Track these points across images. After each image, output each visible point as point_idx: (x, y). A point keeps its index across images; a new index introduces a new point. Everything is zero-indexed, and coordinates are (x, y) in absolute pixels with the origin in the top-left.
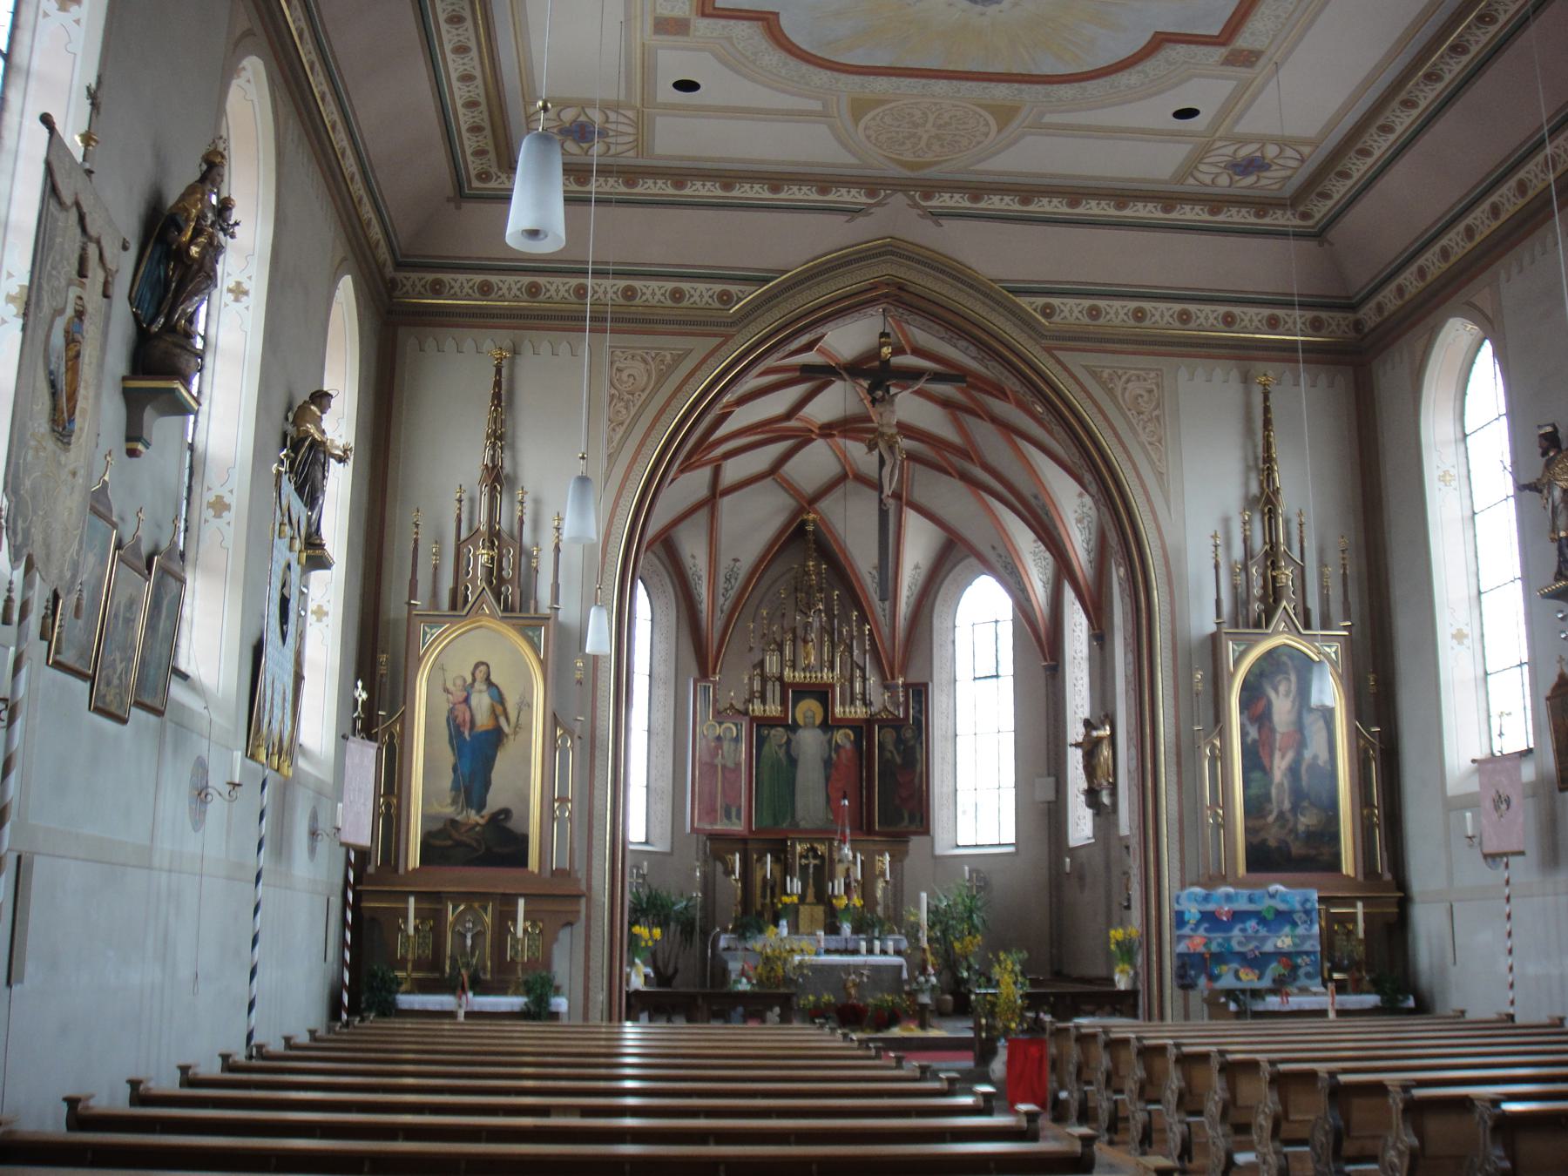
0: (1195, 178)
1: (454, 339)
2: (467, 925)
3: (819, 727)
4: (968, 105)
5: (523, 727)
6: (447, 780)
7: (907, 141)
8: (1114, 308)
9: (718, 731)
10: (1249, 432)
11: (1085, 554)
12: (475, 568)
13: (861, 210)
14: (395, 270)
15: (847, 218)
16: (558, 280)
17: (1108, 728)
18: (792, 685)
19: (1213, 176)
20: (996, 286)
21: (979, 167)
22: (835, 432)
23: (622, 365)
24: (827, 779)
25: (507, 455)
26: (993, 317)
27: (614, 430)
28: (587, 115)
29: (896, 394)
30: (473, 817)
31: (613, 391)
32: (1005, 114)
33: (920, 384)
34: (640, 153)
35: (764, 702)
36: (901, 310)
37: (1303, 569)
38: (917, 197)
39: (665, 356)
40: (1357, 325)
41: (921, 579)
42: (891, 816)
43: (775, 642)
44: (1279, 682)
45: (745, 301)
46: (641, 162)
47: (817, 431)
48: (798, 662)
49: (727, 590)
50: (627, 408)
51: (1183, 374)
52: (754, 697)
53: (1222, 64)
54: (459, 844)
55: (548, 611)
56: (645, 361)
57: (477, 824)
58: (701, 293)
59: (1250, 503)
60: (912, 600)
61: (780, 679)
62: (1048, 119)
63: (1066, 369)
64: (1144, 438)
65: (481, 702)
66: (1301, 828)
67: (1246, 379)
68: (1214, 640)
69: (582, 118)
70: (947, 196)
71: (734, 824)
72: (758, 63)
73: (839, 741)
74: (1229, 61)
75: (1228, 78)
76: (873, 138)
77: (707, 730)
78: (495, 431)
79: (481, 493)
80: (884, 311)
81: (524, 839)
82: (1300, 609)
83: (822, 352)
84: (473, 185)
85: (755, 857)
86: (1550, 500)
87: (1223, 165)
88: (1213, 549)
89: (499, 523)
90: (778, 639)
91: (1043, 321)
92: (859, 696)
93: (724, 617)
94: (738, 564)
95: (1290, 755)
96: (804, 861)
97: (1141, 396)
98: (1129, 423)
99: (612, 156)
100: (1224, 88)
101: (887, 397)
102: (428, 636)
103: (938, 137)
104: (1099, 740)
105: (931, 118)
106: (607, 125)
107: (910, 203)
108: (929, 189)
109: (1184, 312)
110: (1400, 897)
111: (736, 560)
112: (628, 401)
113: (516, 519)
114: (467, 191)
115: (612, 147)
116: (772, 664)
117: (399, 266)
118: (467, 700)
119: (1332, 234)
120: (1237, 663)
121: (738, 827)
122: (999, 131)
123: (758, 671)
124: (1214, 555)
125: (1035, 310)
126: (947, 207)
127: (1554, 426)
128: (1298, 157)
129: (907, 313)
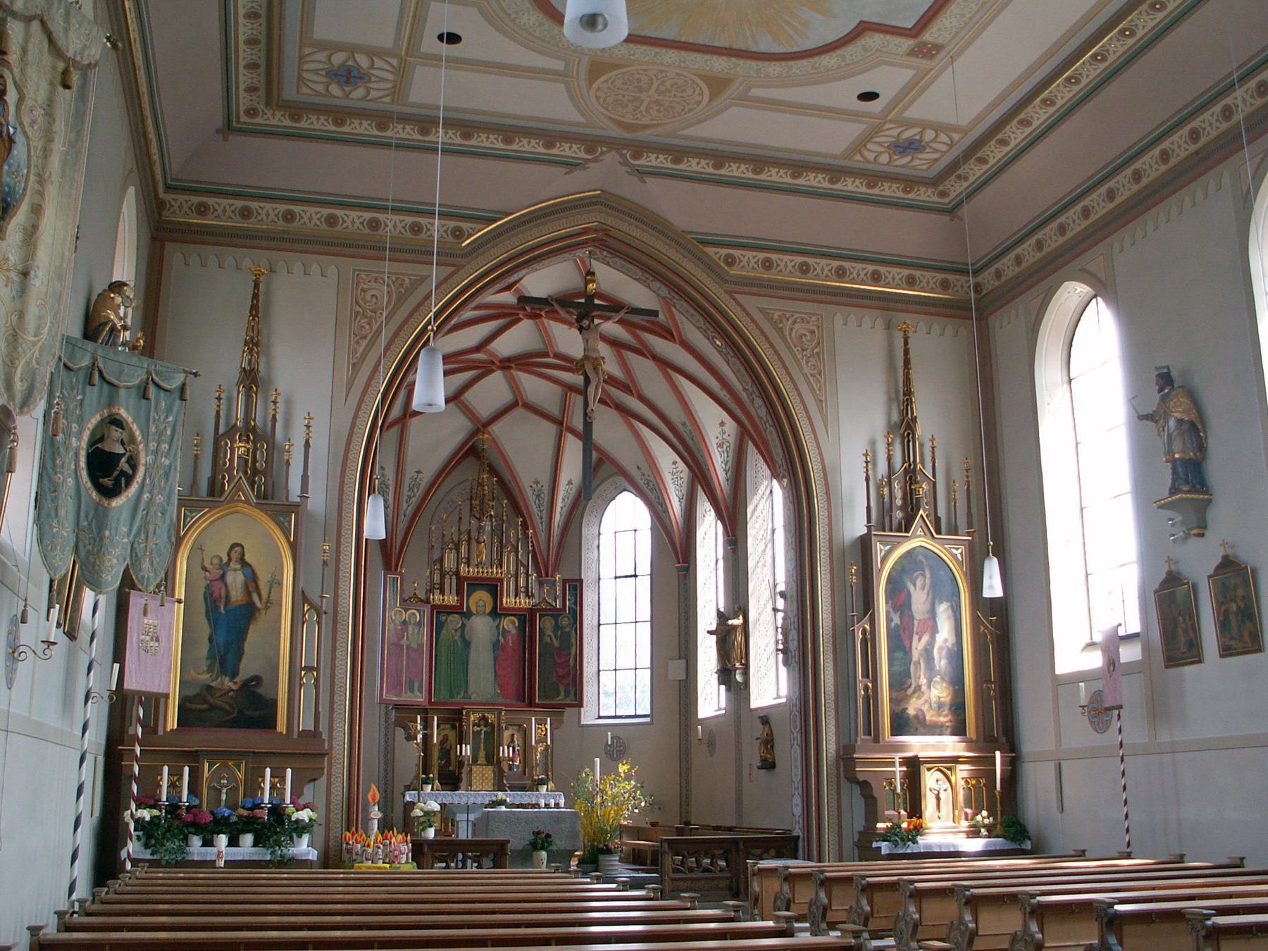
0: (862, 155)
2: (222, 781)
3: (488, 614)
4: (690, 75)
5: (273, 603)
6: (203, 649)
7: (630, 105)
9: (405, 616)
11: (724, 473)
12: (231, 460)
14: (165, 193)
17: (741, 617)
18: (466, 578)
19: (876, 154)
21: (686, 132)
22: (513, 365)
24: (495, 659)
25: (262, 360)
26: (685, 263)
27: (358, 343)
30: (227, 683)
31: (358, 309)
32: (718, 85)
33: (621, 314)
34: (396, 100)
35: (442, 592)
36: (605, 253)
37: (934, 484)
38: (628, 155)
39: (404, 280)
42: (548, 692)
43: (453, 542)
44: (917, 577)
45: (475, 237)
46: (396, 108)
47: (498, 363)
48: (472, 561)
52: (434, 588)
53: (909, 54)
54: (213, 708)
55: (298, 500)
59: (891, 429)
61: (457, 573)
62: (755, 92)
63: (744, 309)
64: (807, 371)
65: (236, 579)
66: (934, 700)
67: (888, 327)
68: (865, 544)
69: (350, 63)
70: (653, 156)
71: (418, 697)
72: (517, 21)
73: (505, 627)
74: (912, 53)
75: (910, 67)
77: (395, 615)
78: (252, 338)
79: (239, 392)
80: (590, 253)
81: (274, 704)
82: (932, 518)
84: (241, 120)
86: (1166, 429)
87: (886, 145)
88: (865, 465)
89: (254, 420)
90: (456, 539)
93: (407, 520)
94: (420, 476)
95: (925, 638)
96: (476, 729)
97: (805, 335)
98: (795, 356)
99: (371, 100)
100: (907, 75)
102: (189, 519)
103: (657, 102)
104: (734, 627)
105: (656, 84)
106: (372, 72)
107: (622, 161)
108: (640, 149)
109: (840, 268)
110: (1012, 757)
111: (418, 472)
112: (371, 317)
113: (270, 417)
114: (234, 124)
115: (372, 92)
116: (450, 561)
117: (168, 188)
119: (965, 210)
120: (884, 560)
121: (420, 698)
122: (710, 100)
123: (438, 566)
126: (652, 167)
127: (1168, 367)
129: (609, 255)
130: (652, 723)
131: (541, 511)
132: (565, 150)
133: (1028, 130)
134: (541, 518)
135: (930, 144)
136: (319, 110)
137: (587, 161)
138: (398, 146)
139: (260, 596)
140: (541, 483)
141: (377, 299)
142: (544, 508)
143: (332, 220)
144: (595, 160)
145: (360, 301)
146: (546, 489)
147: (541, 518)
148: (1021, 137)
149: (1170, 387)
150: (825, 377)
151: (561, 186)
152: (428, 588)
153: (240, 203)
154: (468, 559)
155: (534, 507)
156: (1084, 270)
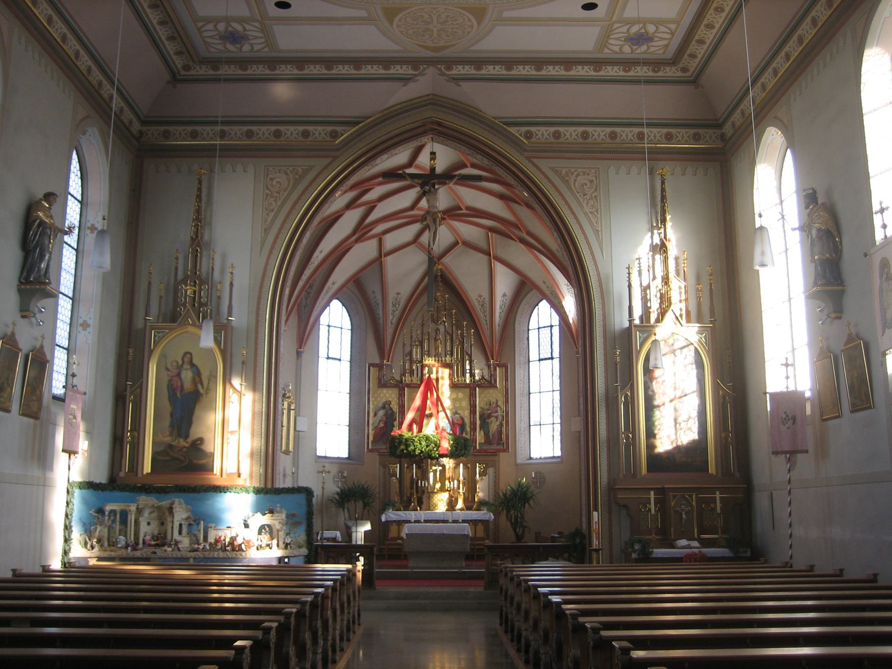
0: (609, 49)
1: (232, 165)
6: (167, 422)
8: (653, 133)
10: (653, 204)
13: (411, 78)
15: (403, 84)
16: (543, 129)
19: (619, 47)
20: (496, 121)
23: (273, 176)
27: (268, 214)
28: (232, 27)
29: (439, 188)
30: (182, 443)
31: (268, 192)
39: (298, 170)
40: (722, 137)
41: (507, 303)
46: (273, 54)
49: (394, 311)
50: (276, 201)
51: (612, 170)
56: (286, 173)
57: (185, 447)
58: (320, 132)
60: (503, 314)
62: (506, 14)
64: (587, 210)
67: (651, 172)
76: (405, 32)
83: (418, 167)
85: (406, 465)
91: (525, 141)
92: (468, 371)
93: (393, 327)
94: (399, 296)
97: (586, 184)
99: (257, 52)
101: (432, 189)
105: (435, 18)
108: (450, 63)
111: (398, 294)
112: (277, 196)
118: (179, 374)
120: (642, 345)
122: (479, 24)
124: (628, 279)
125: (520, 135)
126: (462, 75)
128: (668, 31)
130: (561, 462)
131: (485, 316)
132: (397, 70)
133: (724, 15)
134: (486, 321)
135: (656, 35)
136: (230, 61)
137: (415, 75)
138: (225, 80)
139: (202, 385)
140: (484, 297)
141: (280, 184)
142: (487, 313)
143: (306, 134)
144: (421, 74)
145: (269, 187)
146: (487, 300)
147: (486, 321)
148: (721, 21)
149: (814, 204)
150: (601, 214)
151: (404, 94)
152: (402, 372)
153: (245, 128)
154: (429, 351)
155: (481, 313)
156: (776, 118)
